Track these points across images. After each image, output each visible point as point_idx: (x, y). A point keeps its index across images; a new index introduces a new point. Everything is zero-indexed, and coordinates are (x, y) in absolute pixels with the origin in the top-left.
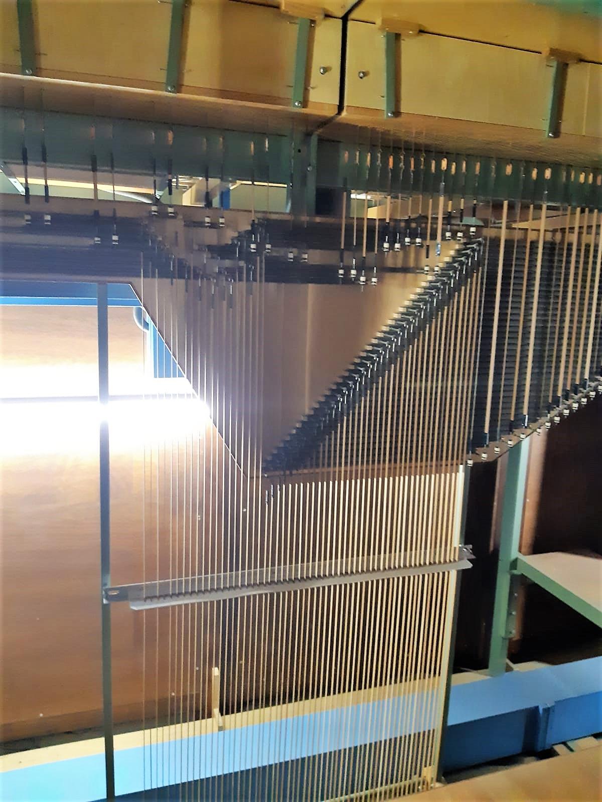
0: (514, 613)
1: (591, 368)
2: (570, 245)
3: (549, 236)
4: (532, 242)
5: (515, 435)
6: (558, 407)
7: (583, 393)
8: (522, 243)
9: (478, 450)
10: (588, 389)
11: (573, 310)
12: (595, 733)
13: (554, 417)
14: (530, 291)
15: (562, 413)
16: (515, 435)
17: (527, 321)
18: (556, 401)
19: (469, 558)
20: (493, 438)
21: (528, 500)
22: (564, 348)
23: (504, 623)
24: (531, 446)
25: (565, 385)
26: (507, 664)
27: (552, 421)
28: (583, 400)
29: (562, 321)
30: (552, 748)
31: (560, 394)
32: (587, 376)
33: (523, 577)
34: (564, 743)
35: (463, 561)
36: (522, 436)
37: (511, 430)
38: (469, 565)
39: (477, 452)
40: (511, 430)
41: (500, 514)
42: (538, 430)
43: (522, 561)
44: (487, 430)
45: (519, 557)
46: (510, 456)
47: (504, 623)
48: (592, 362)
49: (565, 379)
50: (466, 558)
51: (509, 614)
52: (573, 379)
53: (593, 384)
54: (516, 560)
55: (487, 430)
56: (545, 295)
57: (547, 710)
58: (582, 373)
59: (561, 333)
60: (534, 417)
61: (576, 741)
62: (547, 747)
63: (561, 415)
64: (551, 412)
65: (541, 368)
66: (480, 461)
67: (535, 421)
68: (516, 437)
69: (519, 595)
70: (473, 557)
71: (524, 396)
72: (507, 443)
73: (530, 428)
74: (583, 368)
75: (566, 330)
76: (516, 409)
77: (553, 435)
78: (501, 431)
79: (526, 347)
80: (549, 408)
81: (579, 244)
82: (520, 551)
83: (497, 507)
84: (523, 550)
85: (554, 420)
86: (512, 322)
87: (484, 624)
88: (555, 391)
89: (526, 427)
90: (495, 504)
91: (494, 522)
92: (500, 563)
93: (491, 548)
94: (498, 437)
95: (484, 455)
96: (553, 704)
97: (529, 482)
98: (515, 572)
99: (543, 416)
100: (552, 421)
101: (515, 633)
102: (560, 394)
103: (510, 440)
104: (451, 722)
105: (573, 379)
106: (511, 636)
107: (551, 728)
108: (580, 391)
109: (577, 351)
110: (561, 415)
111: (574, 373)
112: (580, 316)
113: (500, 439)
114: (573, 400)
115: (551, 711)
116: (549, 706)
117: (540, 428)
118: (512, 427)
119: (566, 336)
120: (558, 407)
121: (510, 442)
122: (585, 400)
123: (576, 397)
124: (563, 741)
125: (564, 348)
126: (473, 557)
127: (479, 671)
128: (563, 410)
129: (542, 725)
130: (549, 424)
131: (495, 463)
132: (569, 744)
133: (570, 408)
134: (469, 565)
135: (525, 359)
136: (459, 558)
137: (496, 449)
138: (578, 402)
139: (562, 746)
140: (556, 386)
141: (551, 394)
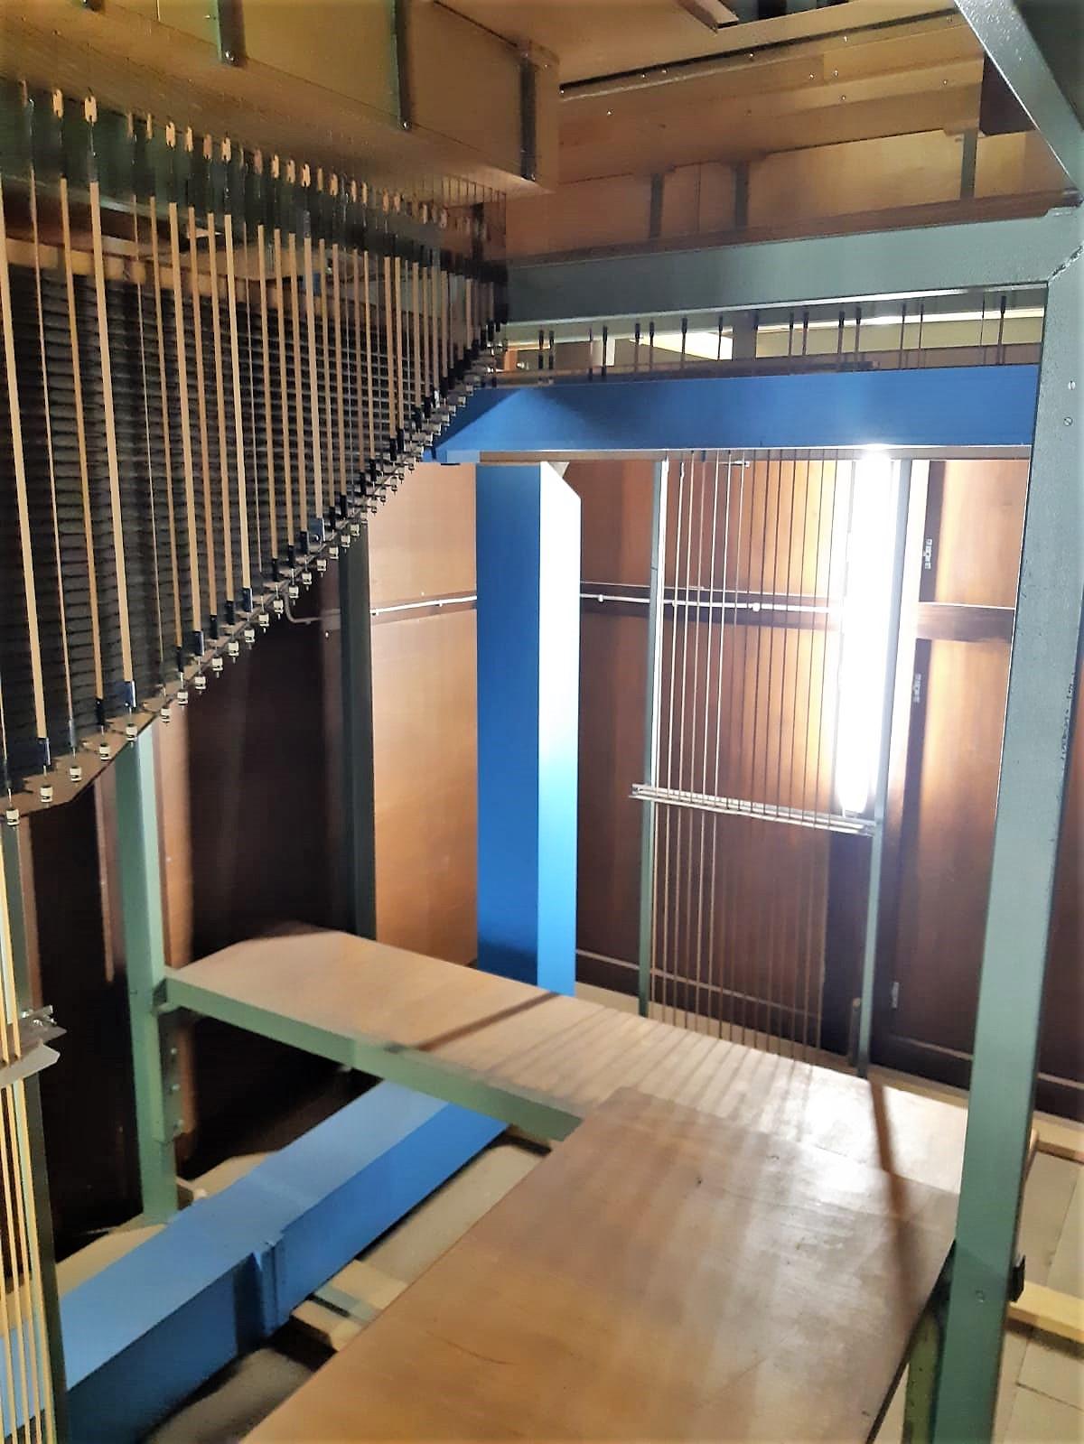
0: (175, 1088)
1: (253, 566)
2: (167, 294)
3: (116, 268)
4: (77, 278)
5: (114, 731)
6: (198, 654)
7: (245, 619)
8: (53, 281)
9: (31, 781)
10: (252, 611)
11: (195, 440)
12: (357, 1253)
13: (193, 678)
14: (91, 395)
15: (258, 624)
16: (114, 731)
17: (97, 465)
18: (193, 643)
19: (49, 1038)
20: (61, 747)
21: (168, 859)
22: (192, 524)
23: (160, 1107)
24: (157, 745)
25: (205, 606)
26: (179, 1187)
27: (190, 687)
28: (319, 563)
29: (177, 466)
30: (292, 1318)
31: (197, 626)
32: (247, 584)
33: (182, 1012)
34: (311, 1297)
35: (34, 1052)
36: (130, 731)
37: (101, 722)
38: (52, 1057)
39: (28, 787)
40: (101, 722)
41: (117, 899)
42: (164, 712)
43: (175, 981)
44: (42, 731)
45: (169, 976)
46: (118, 771)
47: (160, 1107)
48: (252, 554)
49: (204, 594)
50: (41, 1042)
51: (167, 1091)
52: (221, 593)
53: (262, 599)
54: (164, 983)
55: (42, 731)
56: (130, 404)
57: (271, 1254)
58: (238, 578)
59: (179, 493)
60: (152, 681)
61: (330, 1283)
62: (282, 1321)
63: (207, 671)
64: (186, 668)
65: (147, 572)
66: (40, 807)
67: (154, 693)
68: (116, 735)
69: (180, 1049)
70: (60, 1032)
71: (119, 641)
72: (96, 752)
73: (146, 711)
74: (237, 566)
75: (189, 486)
76: (106, 673)
77: (200, 710)
78: (78, 728)
79: (105, 527)
80: (181, 663)
81: (187, 294)
82: (168, 962)
83: (109, 887)
84: (175, 956)
85: (210, 669)
86: (59, 467)
87: (121, 1129)
88: (187, 621)
89: (134, 710)
90: (103, 883)
91: (106, 922)
92: (132, 998)
93: (110, 975)
94: (73, 744)
95: (45, 792)
96: (280, 1237)
97: (166, 824)
98: (166, 1007)
99: (170, 680)
100: (190, 687)
101: (184, 1123)
102: (197, 626)
103: (130, 725)
104: (73, 1378)
105: (221, 593)
106: (180, 1131)
107: (284, 1282)
108: (239, 616)
109: (219, 531)
110: (207, 671)
111: (221, 580)
112: (215, 454)
113: (80, 743)
114: (227, 638)
115: (278, 1255)
116: (273, 1243)
117: (164, 707)
118: (102, 713)
119: (182, 366)
120: (198, 654)
121: (103, 750)
122: (250, 634)
123: (232, 629)
124: (306, 1295)
125: (192, 524)
126: (60, 1032)
127: (124, 1226)
128: (210, 661)
129: (266, 1283)
130: (184, 695)
131: (87, 794)
132: (319, 1294)
133: (224, 654)
134: (52, 1057)
135: (107, 555)
136: (22, 1050)
137: (73, 772)
138: (221, 656)
139: (309, 1305)
140: (186, 610)
141: (178, 631)
